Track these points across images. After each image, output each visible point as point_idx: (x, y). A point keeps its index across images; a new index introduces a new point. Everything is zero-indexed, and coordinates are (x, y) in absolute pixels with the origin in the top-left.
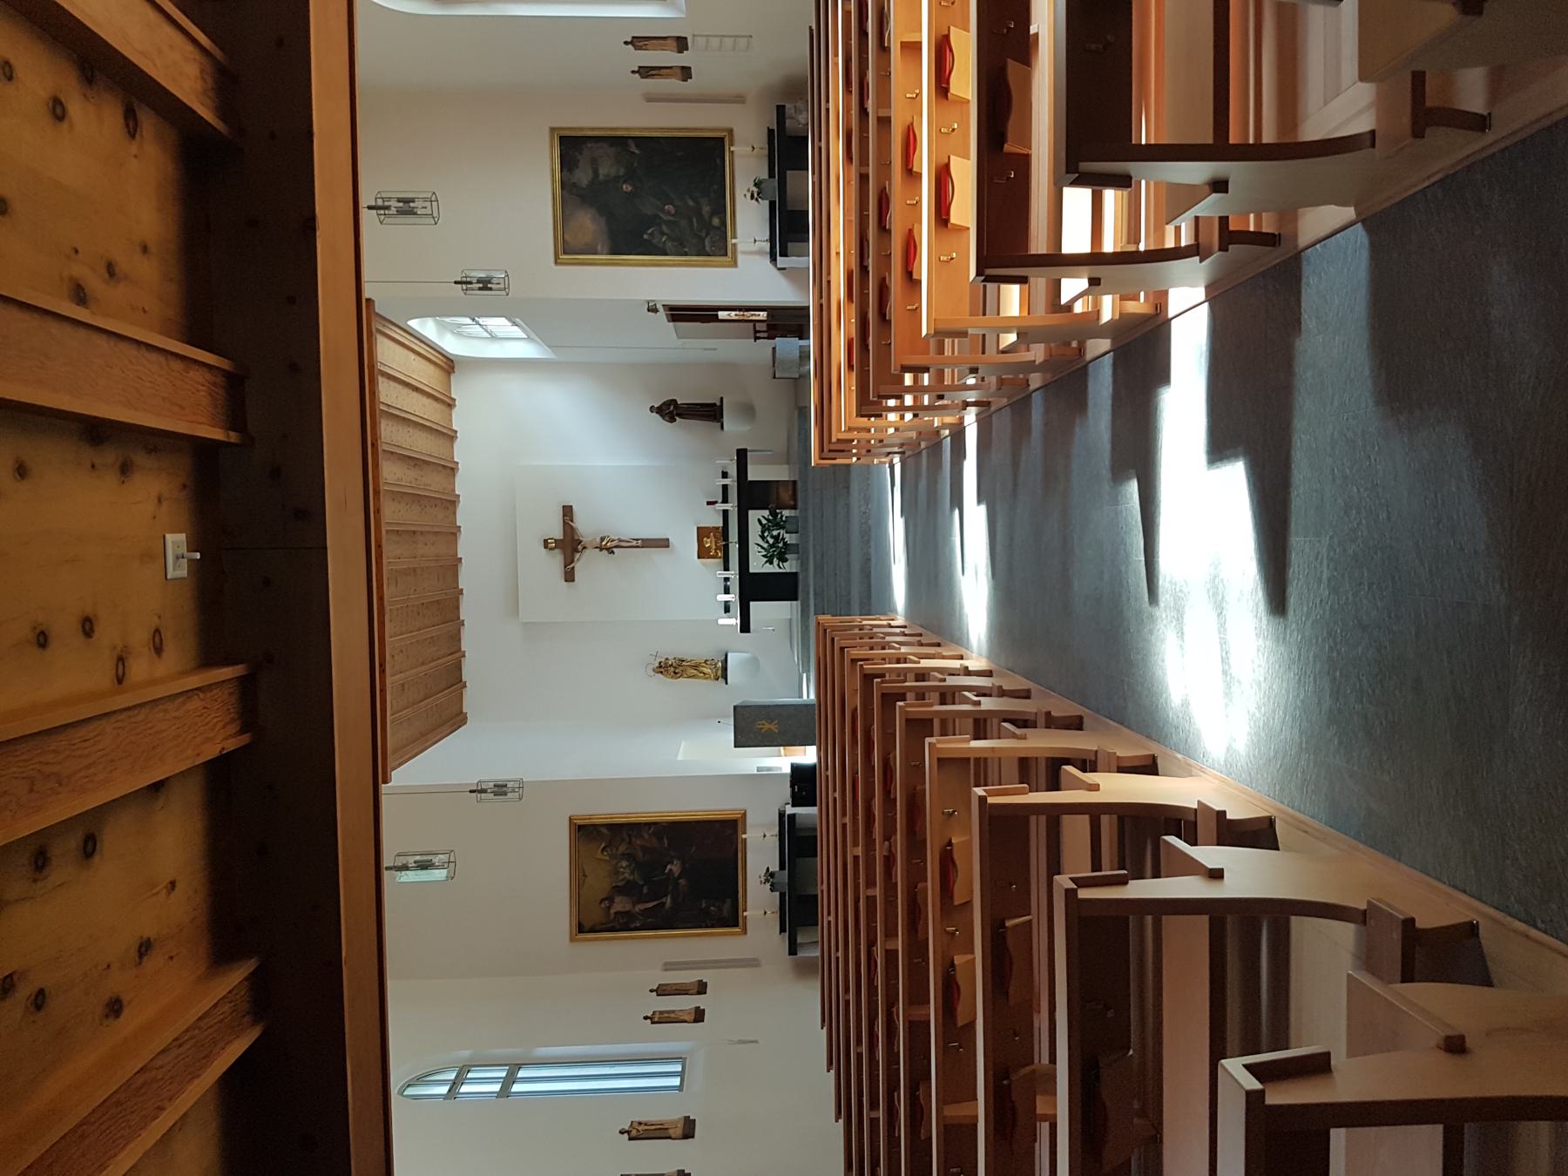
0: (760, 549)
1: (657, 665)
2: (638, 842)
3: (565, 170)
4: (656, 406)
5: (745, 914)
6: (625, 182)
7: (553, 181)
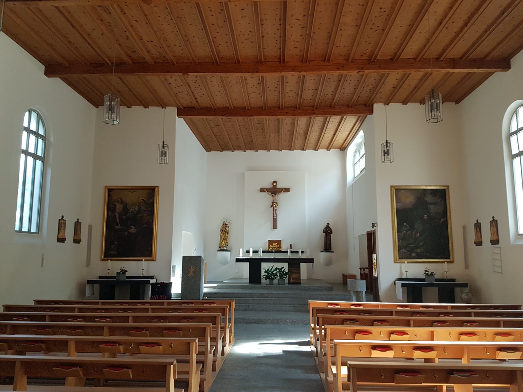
0: (271, 267)
1: (226, 223)
2: (145, 214)
3: (431, 191)
4: (329, 225)
5: (109, 260)
6: (428, 216)
7: (426, 186)
